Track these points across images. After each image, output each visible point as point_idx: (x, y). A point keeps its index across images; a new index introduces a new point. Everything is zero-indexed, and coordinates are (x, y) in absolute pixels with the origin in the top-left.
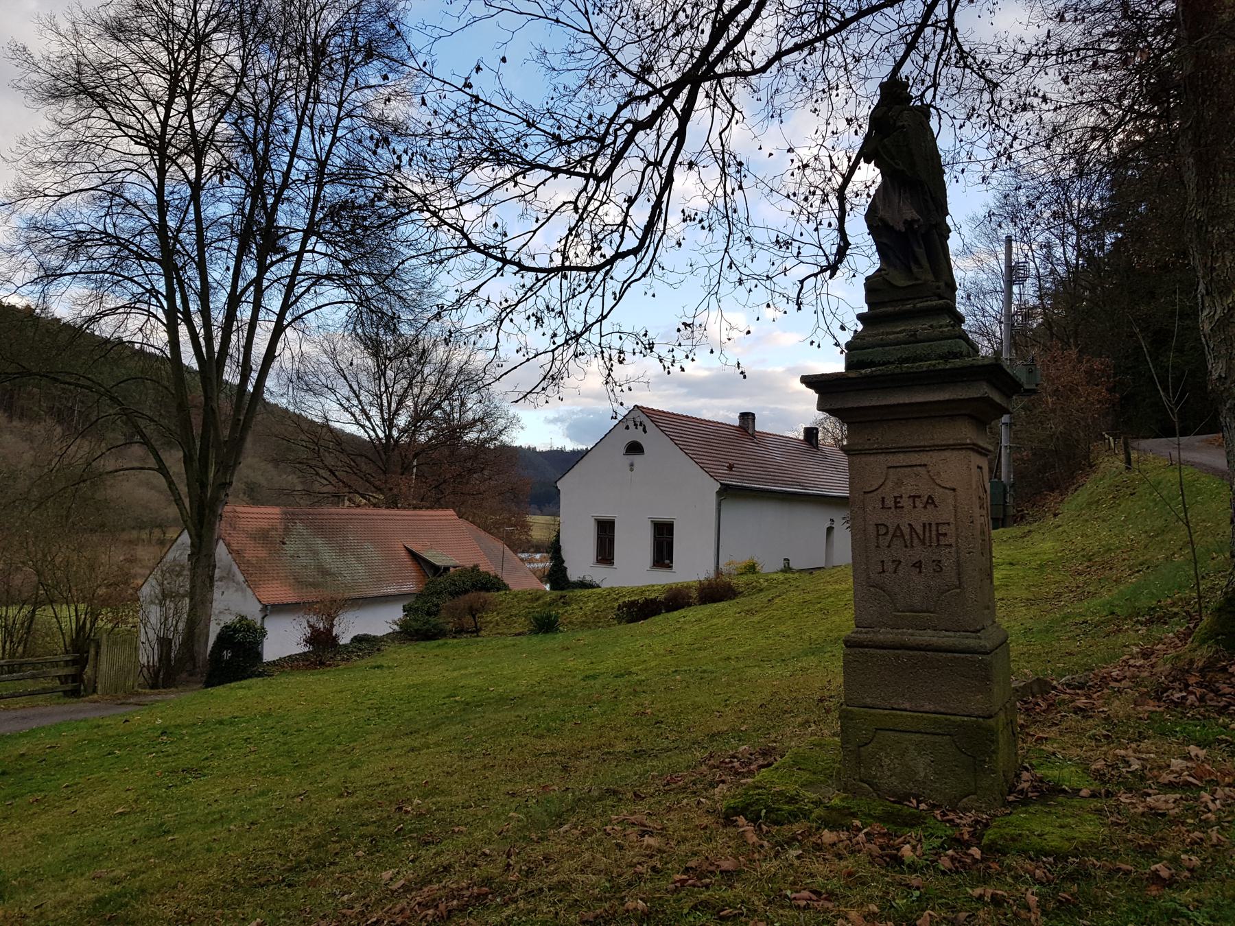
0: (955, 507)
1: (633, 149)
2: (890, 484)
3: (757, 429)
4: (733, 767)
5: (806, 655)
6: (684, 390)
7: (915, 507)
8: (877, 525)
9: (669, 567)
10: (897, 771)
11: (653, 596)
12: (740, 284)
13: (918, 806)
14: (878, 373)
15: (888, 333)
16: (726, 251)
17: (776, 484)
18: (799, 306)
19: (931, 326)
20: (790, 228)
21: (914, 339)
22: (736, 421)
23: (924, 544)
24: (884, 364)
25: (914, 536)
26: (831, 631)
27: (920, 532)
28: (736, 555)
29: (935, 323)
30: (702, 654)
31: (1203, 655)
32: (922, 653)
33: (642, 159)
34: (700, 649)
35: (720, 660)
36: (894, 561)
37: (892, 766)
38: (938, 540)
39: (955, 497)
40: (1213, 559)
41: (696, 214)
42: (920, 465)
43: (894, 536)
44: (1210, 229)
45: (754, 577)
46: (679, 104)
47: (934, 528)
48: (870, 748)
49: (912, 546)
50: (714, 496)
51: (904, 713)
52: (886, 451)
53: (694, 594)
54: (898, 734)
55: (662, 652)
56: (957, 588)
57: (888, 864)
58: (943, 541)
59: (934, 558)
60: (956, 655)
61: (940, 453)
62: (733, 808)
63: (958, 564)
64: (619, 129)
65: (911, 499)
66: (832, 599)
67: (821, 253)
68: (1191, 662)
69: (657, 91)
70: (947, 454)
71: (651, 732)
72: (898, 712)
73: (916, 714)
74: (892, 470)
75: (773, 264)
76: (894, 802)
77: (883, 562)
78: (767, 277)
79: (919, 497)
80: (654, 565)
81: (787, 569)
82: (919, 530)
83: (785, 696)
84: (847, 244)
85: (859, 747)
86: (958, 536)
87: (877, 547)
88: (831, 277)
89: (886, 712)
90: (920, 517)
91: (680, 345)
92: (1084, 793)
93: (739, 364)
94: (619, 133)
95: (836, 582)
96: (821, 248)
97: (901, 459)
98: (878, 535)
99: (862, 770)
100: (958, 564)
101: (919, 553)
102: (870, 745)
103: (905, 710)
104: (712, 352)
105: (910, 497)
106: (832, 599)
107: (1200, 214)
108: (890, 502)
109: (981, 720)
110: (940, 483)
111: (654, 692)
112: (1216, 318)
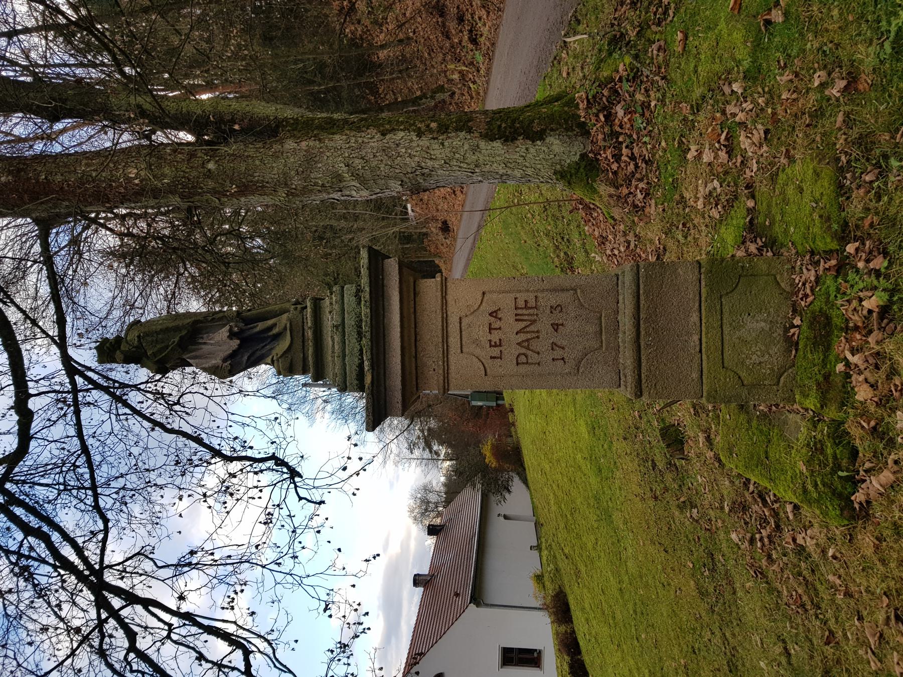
0: (500, 292)
1: (152, 653)
2: (478, 351)
3: (427, 573)
4: (769, 537)
5: (612, 522)
6: (393, 641)
7: (500, 328)
8: (518, 364)
9: (540, 652)
10: (763, 348)
11: (566, 667)
12: (297, 557)
13: (798, 326)
14: (369, 353)
15: (333, 352)
16: (263, 567)
17: (470, 558)
18: (322, 502)
19: (330, 312)
20: (255, 511)
21: (341, 327)
22: (420, 590)
23: (535, 321)
24: (361, 354)
25: (528, 329)
26: (589, 504)
27: (523, 324)
28: (529, 593)
29: (327, 310)
30: (619, 616)
31: (604, 189)
32: (642, 322)
33: (163, 644)
34: (614, 618)
35: (622, 597)
36: (552, 349)
37: (759, 353)
38: (531, 308)
39: (491, 292)
40: (525, 242)
41: (229, 597)
42: (460, 323)
43: (528, 348)
44: (294, 187)
45: (546, 575)
46: (116, 602)
47: (520, 312)
48: (743, 375)
49: (538, 332)
50: (479, 609)
51: (704, 340)
52: (446, 353)
53: (563, 629)
54: (726, 347)
55: (619, 654)
56: (576, 293)
57: (891, 321)
58: (532, 303)
59: (548, 311)
60: (641, 292)
61: (449, 305)
62: (842, 510)
63: (554, 290)
64: (131, 667)
65: (492, 331)
66: (563, 506)
67: (279, 485)
68: (611, 196)
69: (101, 623)
70: (450, 298)
71: (704, 658)
72: (704, 345)
73: (704, 329)
74: (464, 350)
75: (283, 526)
76: (797, 350)
77: (553, 359)
78: (293, 532)
79: (490, 324)
80: (539, 667)
81: (538, 548)
82: (522, 325)
83: (655, 531)
84: (273, 457)
85: (743, 385)
86: (528, 291)
87: (539, 364)
88: (301, 476)
89: (704, 357)
90: (509, 325)
91: (344, 617)
92: (750, 204)
93: (367, 561)
94: (135, 667)
95: (548, 504)
96: (275, 484)
97: (454, 340)
98: (527, 363)
99: (766, 382)
100: (554, 290)
101: (544, 325)
102: (741, 374)
103: (700, 340)
104: (354, 586)
105: (490, 333)
106: (563, 506)
107: (282, 193)
108: (496, 352)
109: (703, 270)
110: (477, 305)
111: (661, 659)
112: (358, 185)
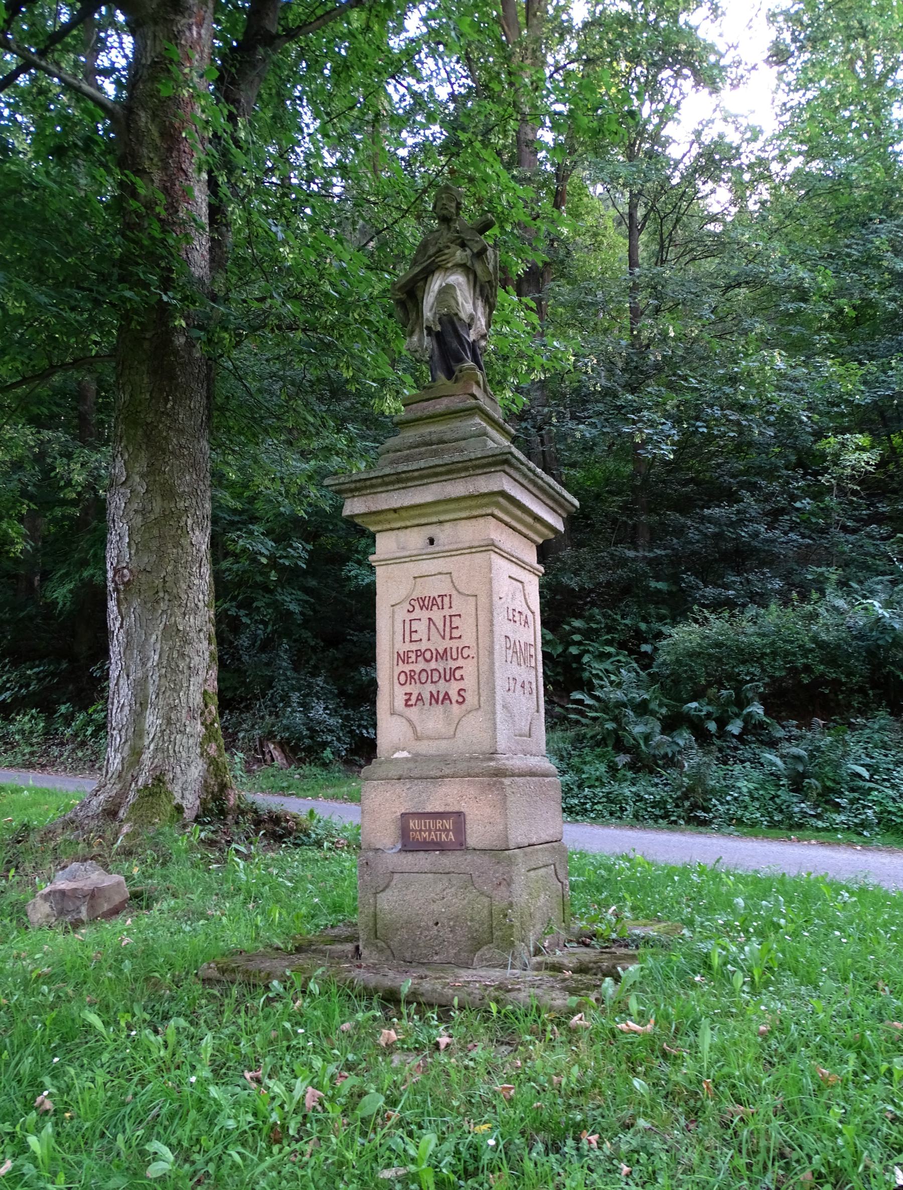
58: (456, 633)
